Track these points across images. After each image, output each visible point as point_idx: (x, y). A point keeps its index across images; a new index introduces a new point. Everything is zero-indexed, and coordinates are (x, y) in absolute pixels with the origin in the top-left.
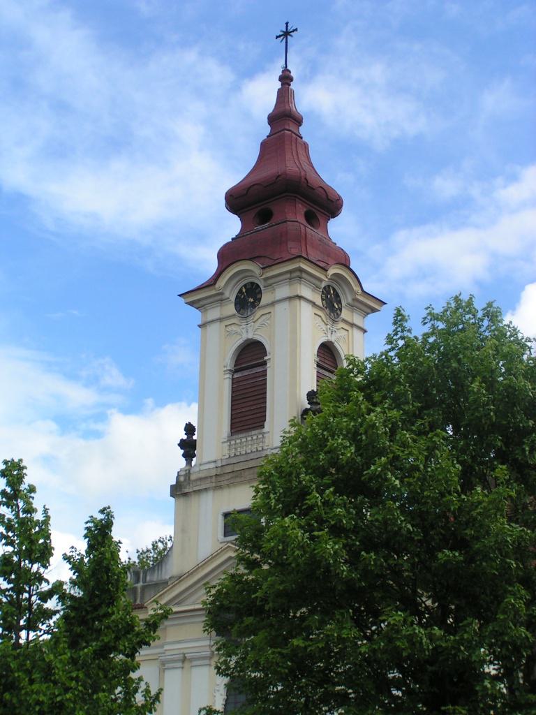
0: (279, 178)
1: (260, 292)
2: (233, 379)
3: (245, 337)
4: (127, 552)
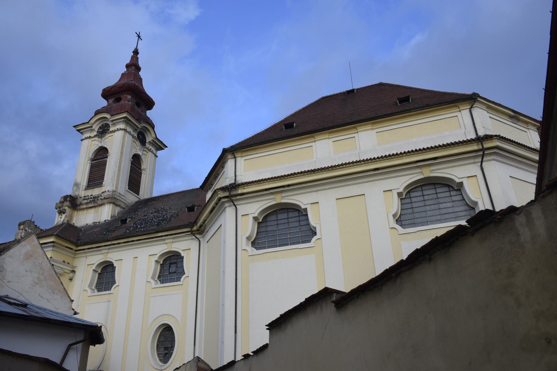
0: (125, 85)
1: (109, 127)
2: (92, 164)
3: (100, 145)
4: (484, 320)
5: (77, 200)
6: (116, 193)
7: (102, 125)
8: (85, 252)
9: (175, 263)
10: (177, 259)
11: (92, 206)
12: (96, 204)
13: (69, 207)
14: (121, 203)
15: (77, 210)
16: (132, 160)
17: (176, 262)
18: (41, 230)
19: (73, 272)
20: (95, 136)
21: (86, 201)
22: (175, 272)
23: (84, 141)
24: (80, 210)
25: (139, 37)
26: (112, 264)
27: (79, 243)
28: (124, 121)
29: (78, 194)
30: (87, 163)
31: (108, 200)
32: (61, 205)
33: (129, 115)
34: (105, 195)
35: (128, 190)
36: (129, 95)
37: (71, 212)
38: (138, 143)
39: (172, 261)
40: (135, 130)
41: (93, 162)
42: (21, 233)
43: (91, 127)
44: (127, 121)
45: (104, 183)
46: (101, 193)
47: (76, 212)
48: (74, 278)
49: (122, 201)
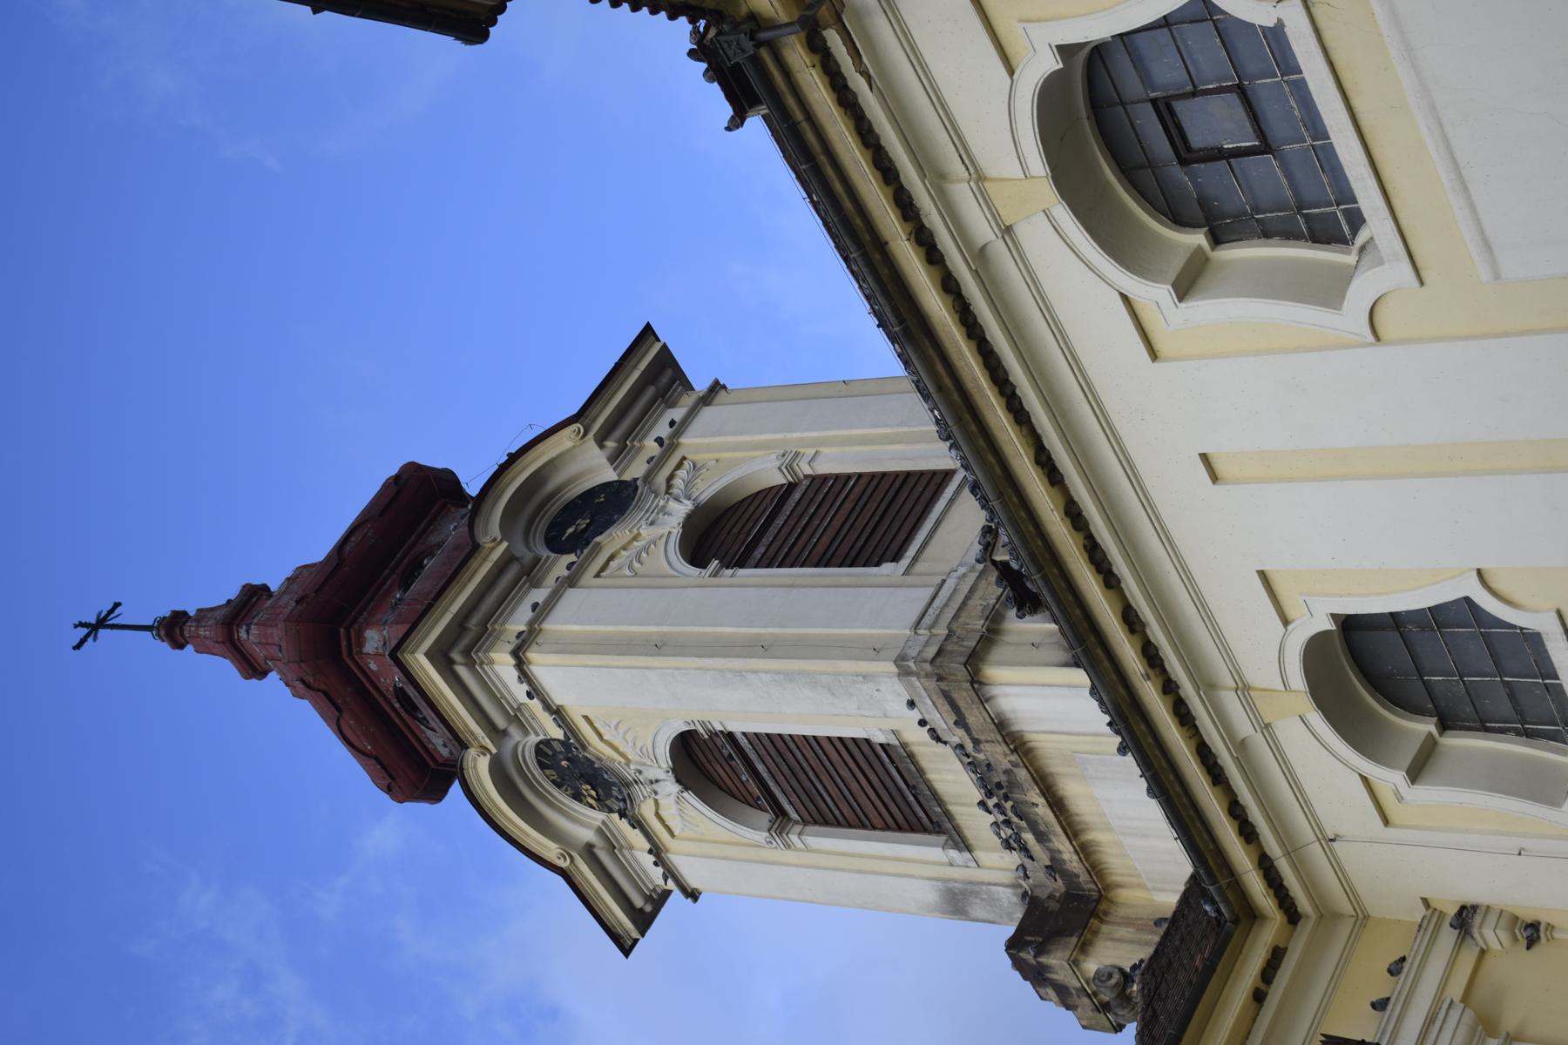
0: (310, 679)
2: (805, 823)
3: (670, 787)
5: (1042, 894)
6: (913, 653)
7: (558, 785)
8: (1287, 854)
9: (1165, 109)
10: (1123, 104)
12: (1022, 774)
13: (1084, 948)
14: (976, 603)
15: (1108, 887)
16: (715, 563)
17: (1154, 102)
19: (1465, 918)
22: (1241, 91)
23: (693, 882)
24: (1096, 869)
26: (1338, 645)
27: (1218, 911)
28: (471, 664)
29: (1009, 891)
30: (807, 849)
31: (961, 704)
32: (1086, 1000)
33: (417, 636)
34: (944, 726)
35: (905, 562)
36: (361, 642)
37: (1123, 932)
38: (614, 538)
39: (1160, 145)
40: (531, 574)
45: (879, 738)
46: (948, 750)
47: (1123, 895)
48: (1518, 912)
49: (967, 598)
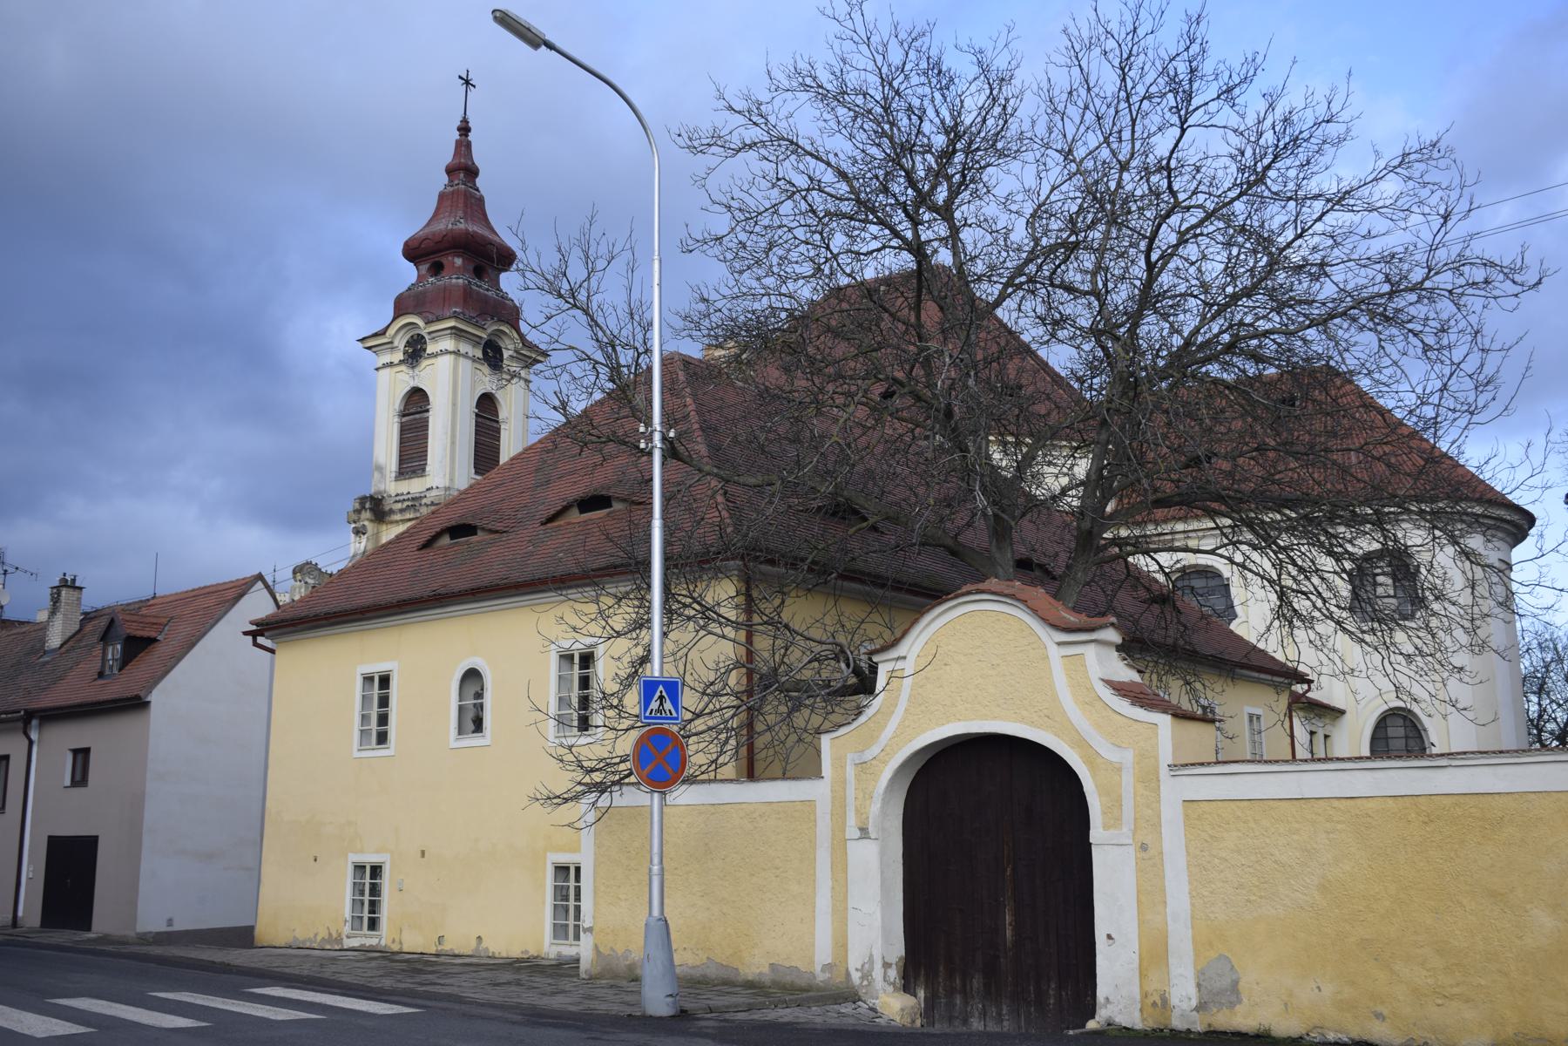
1: (425, 343)
3: (413, 384)
4: (423, 853)
11: (411, 516)
13: (371, 521)
18: (331, 575)
20: (401, 362)
21: (399, 506)
25: (467, 82)
36: (458, 256)
38: (486, 369)
40: (476, 344)
41: (404, 419)
42: (300, 588)
43: (391, 343)
44: (457, 333)
47: (384, 527)
